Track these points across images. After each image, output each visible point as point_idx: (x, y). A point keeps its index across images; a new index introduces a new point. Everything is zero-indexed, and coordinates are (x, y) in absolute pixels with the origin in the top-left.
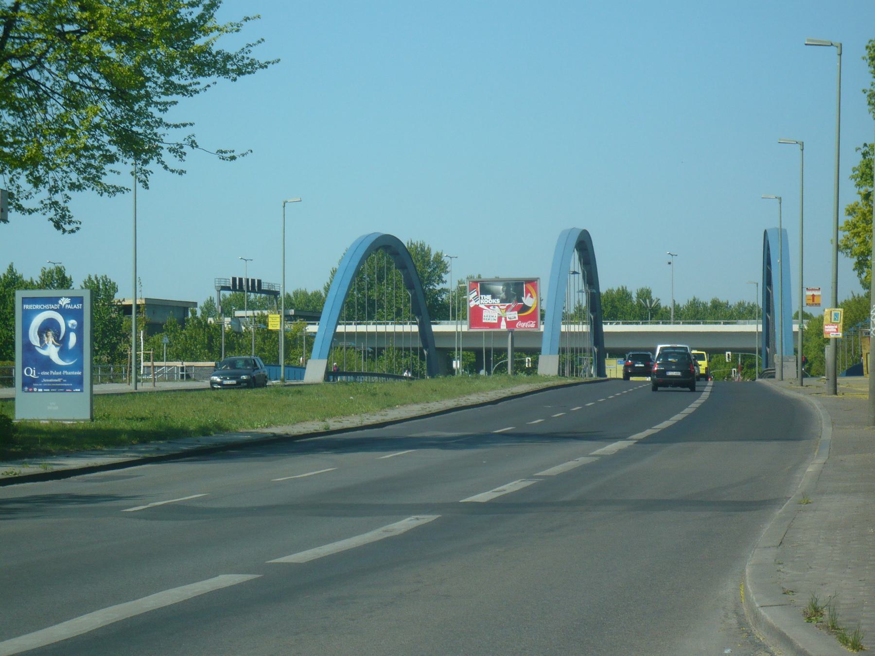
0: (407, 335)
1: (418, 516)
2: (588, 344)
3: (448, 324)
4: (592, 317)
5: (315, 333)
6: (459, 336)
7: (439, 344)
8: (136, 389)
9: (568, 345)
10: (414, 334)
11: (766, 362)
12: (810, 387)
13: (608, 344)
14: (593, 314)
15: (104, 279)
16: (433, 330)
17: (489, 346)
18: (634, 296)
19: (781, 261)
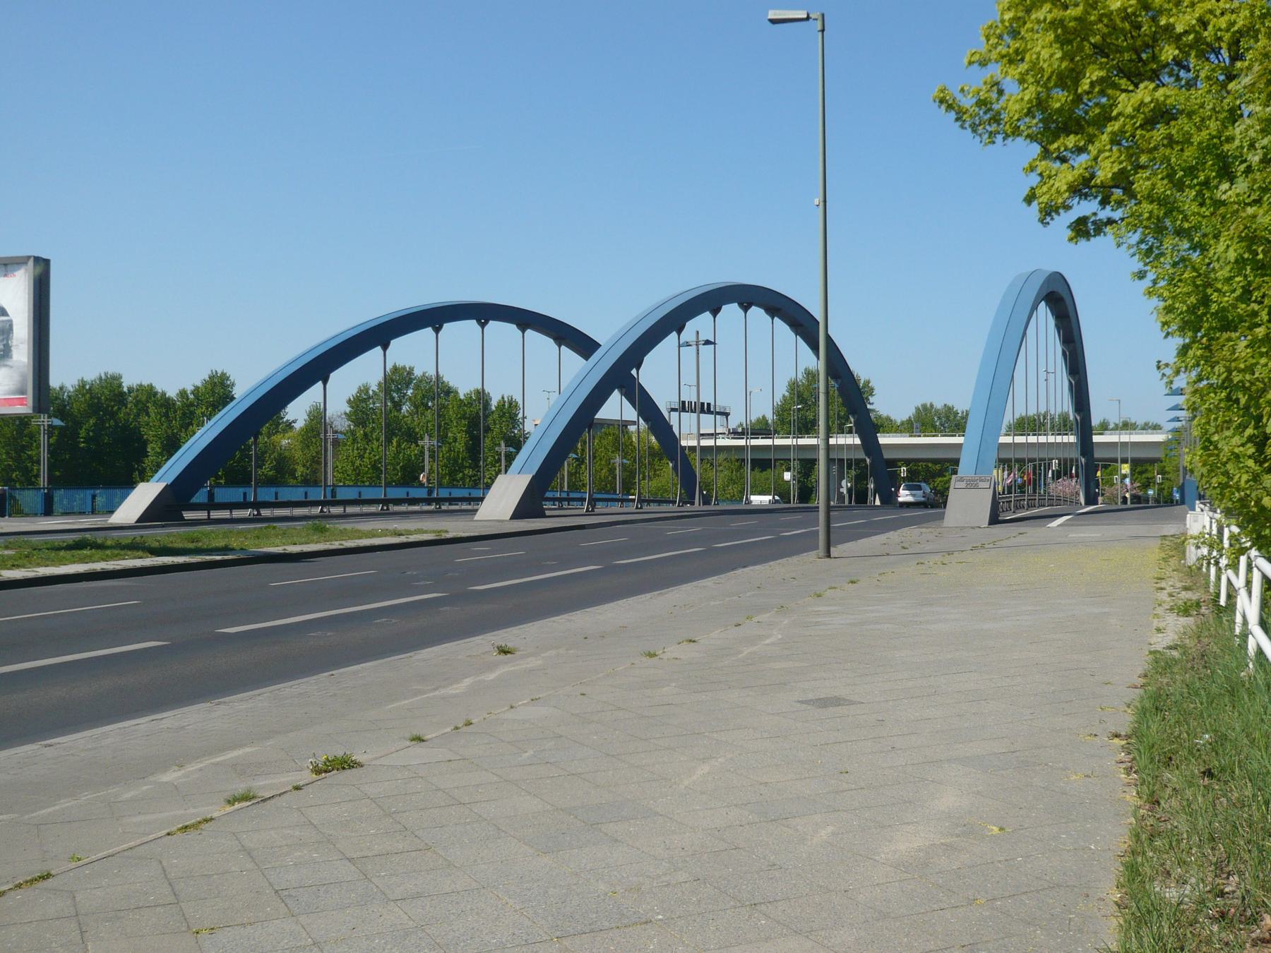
0: (849, 447)
1: (331, 673)
2: (1075, 454)
3: (1146, 434)
4: (1078, 418)
5: (962, 444)
6: (794, 449)
7: (887, 455)
8: (276, 499)
9: (1004, 455)
10: (855, 446)
11: (499, 534)
12: (58, 746)
13: (1098, 454)
14: (1079, 414)
15: (1042, 417)
16: (1094, 441)
17: (850, 457)
18: (862, 382)
19: (825, 201)
